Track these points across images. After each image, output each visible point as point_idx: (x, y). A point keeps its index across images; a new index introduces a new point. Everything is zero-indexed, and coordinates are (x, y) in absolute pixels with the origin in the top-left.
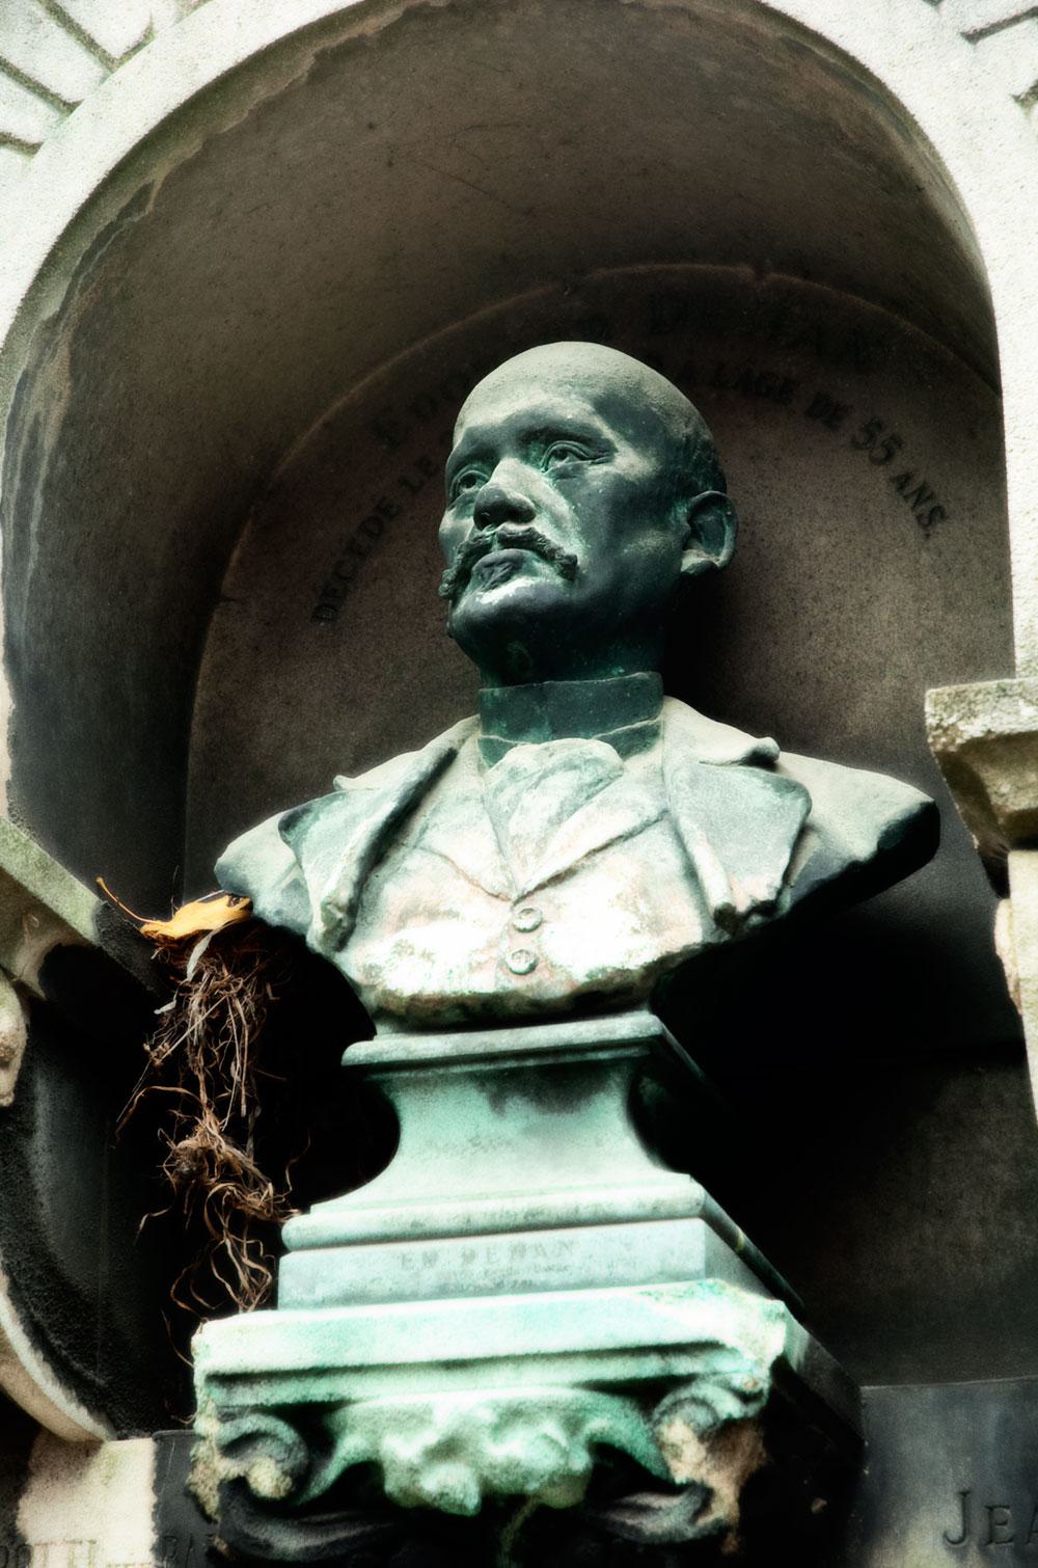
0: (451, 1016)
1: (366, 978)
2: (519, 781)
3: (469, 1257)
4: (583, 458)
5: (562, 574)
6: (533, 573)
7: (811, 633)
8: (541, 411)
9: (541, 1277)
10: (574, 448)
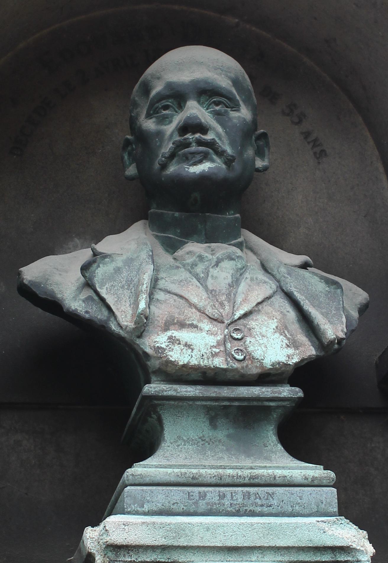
0: (195, 376)
1: (156, 353)
2: (204, 262)
3: (222, 496)
4: (227, 107)
5: (225, 163)
6: (213, 161)
7: (265, 201)
8: (210, 81)
9: (259, 509)
10: (225, 102)
